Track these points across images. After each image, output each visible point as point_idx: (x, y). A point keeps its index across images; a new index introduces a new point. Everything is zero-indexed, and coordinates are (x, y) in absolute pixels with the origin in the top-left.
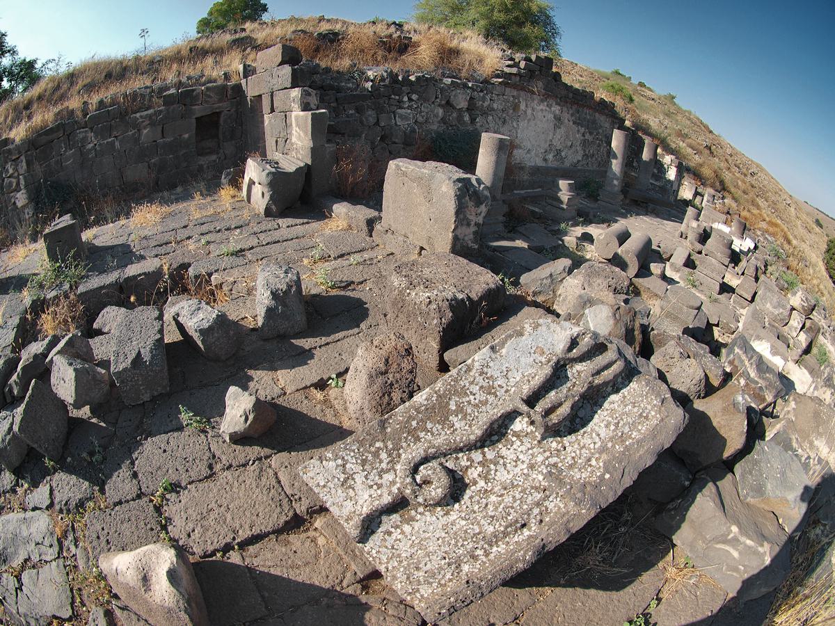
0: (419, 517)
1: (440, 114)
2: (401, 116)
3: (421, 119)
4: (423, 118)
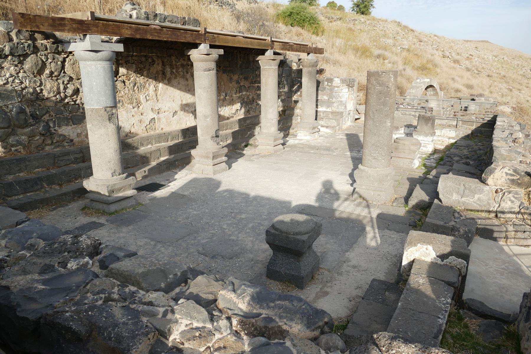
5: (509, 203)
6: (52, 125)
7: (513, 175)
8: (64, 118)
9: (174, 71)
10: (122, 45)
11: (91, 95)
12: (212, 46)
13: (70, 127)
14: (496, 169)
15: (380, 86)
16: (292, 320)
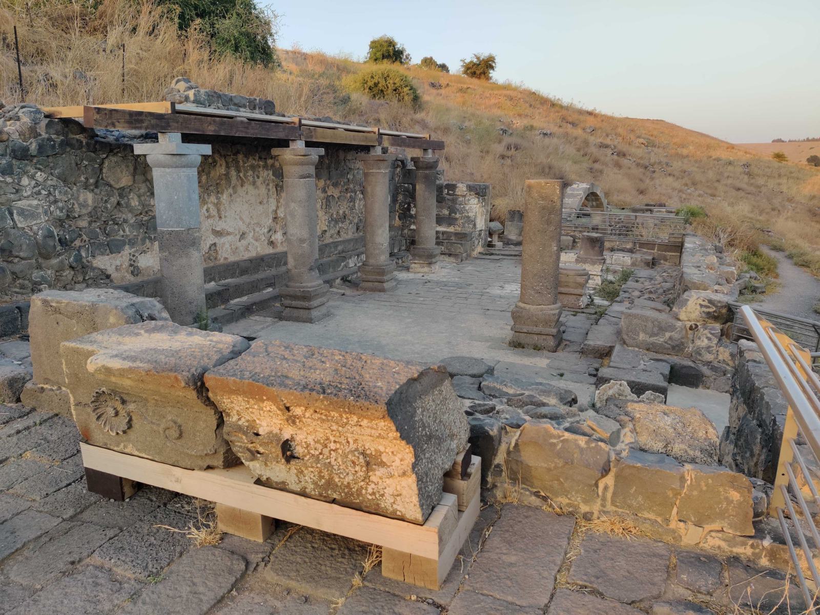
0: (372, 449)
1: (90, 202)
2: (22, 212)
3: (58, 212)
4: (61, 211)
5: (706, 341)
6: (84, 254)
7: (709, 307)
8: (100, 244)
9: (241, 175)
10: (210, 146)
11: (170, 213)
12: (309, 144)
13: (106, 258)
14: (688, 300)
15: (543, 200)
16: (548, 396)
